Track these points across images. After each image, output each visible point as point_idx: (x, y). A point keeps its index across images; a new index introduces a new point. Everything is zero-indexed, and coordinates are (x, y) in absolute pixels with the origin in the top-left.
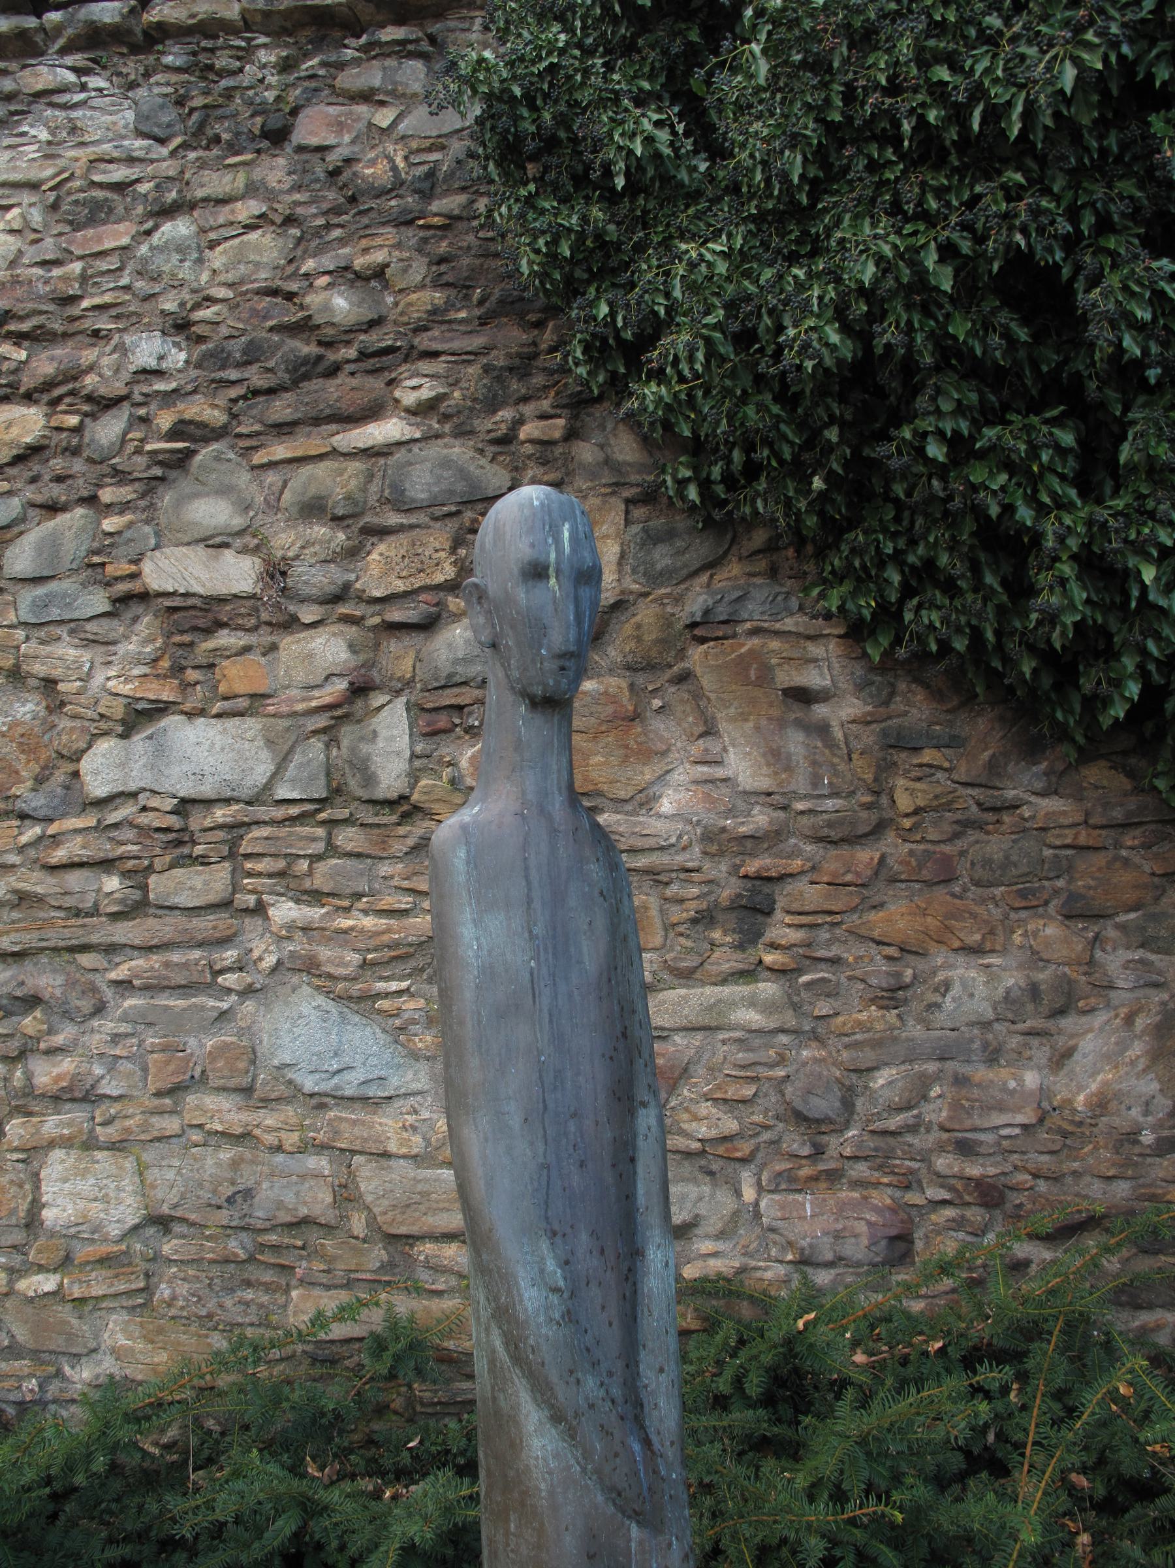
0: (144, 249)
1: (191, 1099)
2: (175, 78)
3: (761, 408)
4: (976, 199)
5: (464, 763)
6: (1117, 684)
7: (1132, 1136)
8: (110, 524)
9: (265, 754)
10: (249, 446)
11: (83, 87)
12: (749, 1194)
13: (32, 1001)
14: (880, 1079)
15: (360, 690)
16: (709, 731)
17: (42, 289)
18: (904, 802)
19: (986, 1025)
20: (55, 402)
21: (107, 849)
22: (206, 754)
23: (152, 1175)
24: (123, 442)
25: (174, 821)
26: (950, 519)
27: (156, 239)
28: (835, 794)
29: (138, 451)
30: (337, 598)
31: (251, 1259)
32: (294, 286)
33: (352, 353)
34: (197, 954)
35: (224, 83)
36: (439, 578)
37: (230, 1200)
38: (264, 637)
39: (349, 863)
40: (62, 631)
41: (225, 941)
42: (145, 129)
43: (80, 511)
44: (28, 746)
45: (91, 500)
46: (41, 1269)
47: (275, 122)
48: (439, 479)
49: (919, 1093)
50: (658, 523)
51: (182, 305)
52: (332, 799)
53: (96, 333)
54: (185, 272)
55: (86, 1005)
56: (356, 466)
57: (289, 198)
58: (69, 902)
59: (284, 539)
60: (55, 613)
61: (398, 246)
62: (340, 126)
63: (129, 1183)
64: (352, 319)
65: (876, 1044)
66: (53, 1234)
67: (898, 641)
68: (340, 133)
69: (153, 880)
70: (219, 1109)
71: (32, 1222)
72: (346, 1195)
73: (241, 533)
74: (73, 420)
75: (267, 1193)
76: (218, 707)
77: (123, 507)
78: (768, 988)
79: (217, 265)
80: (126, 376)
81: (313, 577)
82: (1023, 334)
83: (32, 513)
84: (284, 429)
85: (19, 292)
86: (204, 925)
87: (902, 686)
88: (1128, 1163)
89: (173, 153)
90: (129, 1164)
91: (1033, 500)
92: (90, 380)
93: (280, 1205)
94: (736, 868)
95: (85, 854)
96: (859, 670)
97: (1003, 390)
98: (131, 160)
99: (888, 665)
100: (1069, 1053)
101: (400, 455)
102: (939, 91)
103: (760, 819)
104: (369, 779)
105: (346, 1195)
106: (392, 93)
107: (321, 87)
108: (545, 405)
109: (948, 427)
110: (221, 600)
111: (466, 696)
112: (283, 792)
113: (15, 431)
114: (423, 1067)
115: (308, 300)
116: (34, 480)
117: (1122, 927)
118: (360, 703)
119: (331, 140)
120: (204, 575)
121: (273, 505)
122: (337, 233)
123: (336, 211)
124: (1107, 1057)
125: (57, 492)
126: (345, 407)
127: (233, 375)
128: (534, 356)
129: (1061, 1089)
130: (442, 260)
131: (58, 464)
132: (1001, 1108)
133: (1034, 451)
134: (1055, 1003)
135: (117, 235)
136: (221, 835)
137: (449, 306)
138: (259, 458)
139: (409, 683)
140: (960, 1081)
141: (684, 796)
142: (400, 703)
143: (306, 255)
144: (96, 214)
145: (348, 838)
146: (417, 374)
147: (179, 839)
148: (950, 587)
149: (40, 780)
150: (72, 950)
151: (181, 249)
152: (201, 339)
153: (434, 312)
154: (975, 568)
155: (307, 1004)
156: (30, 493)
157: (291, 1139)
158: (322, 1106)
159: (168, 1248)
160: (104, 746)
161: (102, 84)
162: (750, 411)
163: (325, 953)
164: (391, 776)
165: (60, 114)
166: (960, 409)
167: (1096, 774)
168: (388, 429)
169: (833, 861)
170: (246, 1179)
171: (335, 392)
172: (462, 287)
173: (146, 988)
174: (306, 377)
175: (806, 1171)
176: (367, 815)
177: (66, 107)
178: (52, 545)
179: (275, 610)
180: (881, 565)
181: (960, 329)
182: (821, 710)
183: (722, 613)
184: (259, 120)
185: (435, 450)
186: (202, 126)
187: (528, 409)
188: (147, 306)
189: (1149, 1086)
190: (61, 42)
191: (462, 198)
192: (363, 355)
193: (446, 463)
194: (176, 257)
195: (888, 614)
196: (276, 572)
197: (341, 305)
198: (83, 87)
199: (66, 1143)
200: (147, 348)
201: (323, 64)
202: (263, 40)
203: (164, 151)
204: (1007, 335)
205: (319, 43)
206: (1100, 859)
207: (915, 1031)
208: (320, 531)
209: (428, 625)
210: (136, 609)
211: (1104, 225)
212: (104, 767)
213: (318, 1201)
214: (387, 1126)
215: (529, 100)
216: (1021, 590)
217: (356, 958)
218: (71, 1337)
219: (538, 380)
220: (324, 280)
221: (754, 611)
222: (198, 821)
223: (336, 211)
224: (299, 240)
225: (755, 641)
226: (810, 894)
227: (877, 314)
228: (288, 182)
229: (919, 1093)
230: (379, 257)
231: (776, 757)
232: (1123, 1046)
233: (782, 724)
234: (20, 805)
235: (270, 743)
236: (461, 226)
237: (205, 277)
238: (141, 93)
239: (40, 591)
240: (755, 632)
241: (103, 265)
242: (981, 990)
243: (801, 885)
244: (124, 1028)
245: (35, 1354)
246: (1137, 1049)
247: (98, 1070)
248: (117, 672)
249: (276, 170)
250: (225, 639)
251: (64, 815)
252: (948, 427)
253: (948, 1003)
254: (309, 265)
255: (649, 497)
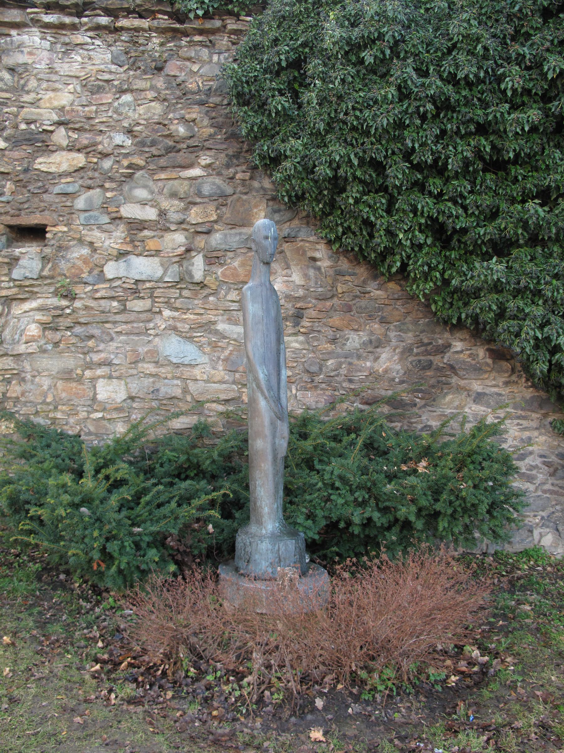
0: (116, 104)
1: (140, 365)
2: (125, 45)
3: (308, 183)
4: (364, 143)
5: (219, 273)
6: (395, 262)
7: (393, 379)
8: (109, 195)
9: (160, 268)
10: (152, 173)
11: (93, 44)
12: (294, 391)
13: (92, 337)
14: (330, 362)
15: (188, 251)
16: (288, 267)
17: (82, 114)
18: (340, 290)
19: (358, 350)
20: (88, 153)
21: (113, 294)
22: (143, 267)
23: (130, 385)
24: (112, 168)
25: (134, 286)
26: (356, 218)
27: (120, 101)
28: (321, 287)
29: (117, 172)
30: (181, 223)
31: (159, 409)
32: (166, 122)
33: (185, 146)
34: (141, 324)
35: (142, 48)
36: (212, 219)
37: (153, 392)
38: (159, 233)
39: (186, 300)
40: (94, 227)
41: (149, 321)
42: (115, 61)
43: (98, 190)
44: (86, 261)
45: (102, 186)
46: (97, 411)
47: (159, 64)
48: (212, 189)
49: (339, 365)
50: (276, 207)
51: (130, 125)
52: (184, 281)
53: (101, 131)
54: (130, 114)
55: (108, 338)
56: (186, 182)
57: (164, 92)
58: (101, 309)
59: (165, 204)
60: (92, 222)
61: (200, 112)
62: (181, 69)
63: (123, 388)
64: (185, 135)
65: (329, 353)
66: (100, 402)
67: (340, 246)
68: (181, 72)
69: (128, 303)
70: (150, 368)
71: (94, 399)
72: (185, 391)
73: (151, 201)
74: (95, 160)
75: (163, 390)
76: (146, 253)
77: (113, 190)
78: (301, 338)
79: (141, 112)
80: (111, 147)
81: (174, 216)
82: (374, 175)
83: (82, 189)
84: (163, 169)
85: (74, 114)
86: (143, 316)
87: (341, 258)
88: (392, 386)
89: (125, 71)
90: (123, 382)
91: (374, 215)
92: (100, 147)
93: (166, 393)
94: (294, 306)
95: (107, 295)
96: (330, 252)
97: (369, 187)
98: (111, 72)
99: (337, 252)
100: (378, 358)
101: (200, 180)
102: (357, 118)
103: (301, 292)
104: (192, 277)
105: (185, 391)
106: (198, 59)
107: (174, 54)
108: (244, 168)
109: (354, 195)
110: (146, 221)
111: (220, 254)
112: (167, 279)
113: (75, 162)
114: (207, 356)
115: (171, 127)
116: (82, 178)
117: (395, 326)
118: (188, 255)
119: (178, 74)
120: (140, 213)
121: (161, 192)
122: (180, 106)
123: (180, 98)
124: (388, 359)
125: (90, 182)
126: (183, 163)
127: (147, 149)
128: (240, 153)
129: (376, 366)
130: (213, 118)
131: (90, 174)
132: (360, 371)
133: (375, 204)
134: (376, 344)
135: (108, 98)
136: (148, 291)
137: (215, 134)
138: (156, 177)
139: (203, 249)
140: (350, 364)
141: (280, 285)
142: (201, 255)
143: (170, 112)
144: (99, 90)
145: (186, 293)
146: (205, 155)
147: (135, 291)
148: (354, 233)
149: (90, 272)
150: (103, 322)
151: (128, 104)
152: (136, 136)
153: (210, 135)
154: (361, 229)
155: (174, 339)
156: (80, 182)
157: (169, 376)
158: (178, 367)
159: (135, 405)
160: (111, 263)
161: (100, 43)
162: (305, 183)
163: (179, 325)
164: (198, 275)
165: (86, 52)
166: (358, 191)
167: (391, 285)
168: (196, 172)
169: (320, 305)
170: (157, 386)
171: (180, 158)
172: (219, 127)
173: (126, 334)
174: (170, 152)
175: (309, 386)
176: (190, 286)
177: (87, 50)
178: (89, 201)
179: (162, 225)
180: (337, 225)
181: (358, 173)
182: (319, 263)
183: (293, 234)
184: (154, 64)
185: (210, 179)
186: (134, 63)
187: (238, 169)
188: (118, 123)
189: (399, 367)
190: (86, 28)
191: (219, 99)
192: (188, 147)
193: (214, 184)
194: (127, 108)
195: (338, 239)
196: (162, 213)
197: (182, 130)
198: (93, 44)
199: (103, 377)
200: (119, 138)
201: (175, 46)
202: (154, 35)
203: (122, 70)
204: (370, 175)
205: (173, 38)
206: (390, 308)
207: (339, 350)
208: (176, 202)
209: (208, 233)
210: (118, 221)
211: (393, 153)
212: (111, 270)
213: (178, 392)
214: (197, 372)
215: (247, 82)
216: (371, 236)
217: (188, 327)
218: (107, 429)
219: (242, 160)
220: (176, 122)
221: (302, 235)
222: (140, 287)
223: (180, 98)
224: (167, 107)
225: (302, 243)
226: (312, 313)
227: (339, 167)
228: (164, 86)
229: (339, 365)
230: (194, 116)
231: (306, 276)
232: (392, 356)
233: (308, 267)
234: (84, 280)
235: (162, 265)
236: (219, 107)
237: (137, 116)
238: (113, 48)
239: (87, 214)
240: (302, 240)
241: (103, 108)
242: (357, 341)
243: (311, 311)
244: (120, 345)
245: (96, 435)
246: (396, 357)
247: (112, 357)
248: (114, 240)
249: (160, 82)
250: (146, 233)
251: (98, 284)
252: (354, 195)
253: (348, 344)
254: (171, 116)
255: (274, 199)
